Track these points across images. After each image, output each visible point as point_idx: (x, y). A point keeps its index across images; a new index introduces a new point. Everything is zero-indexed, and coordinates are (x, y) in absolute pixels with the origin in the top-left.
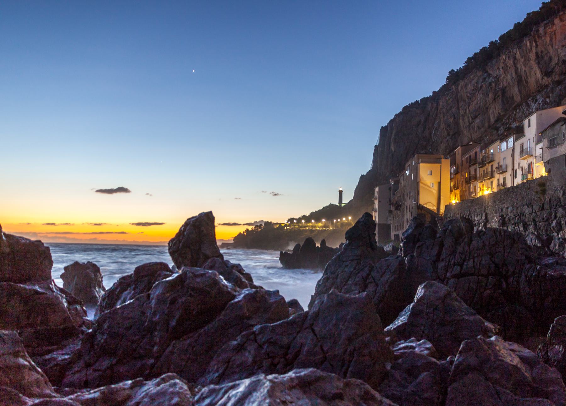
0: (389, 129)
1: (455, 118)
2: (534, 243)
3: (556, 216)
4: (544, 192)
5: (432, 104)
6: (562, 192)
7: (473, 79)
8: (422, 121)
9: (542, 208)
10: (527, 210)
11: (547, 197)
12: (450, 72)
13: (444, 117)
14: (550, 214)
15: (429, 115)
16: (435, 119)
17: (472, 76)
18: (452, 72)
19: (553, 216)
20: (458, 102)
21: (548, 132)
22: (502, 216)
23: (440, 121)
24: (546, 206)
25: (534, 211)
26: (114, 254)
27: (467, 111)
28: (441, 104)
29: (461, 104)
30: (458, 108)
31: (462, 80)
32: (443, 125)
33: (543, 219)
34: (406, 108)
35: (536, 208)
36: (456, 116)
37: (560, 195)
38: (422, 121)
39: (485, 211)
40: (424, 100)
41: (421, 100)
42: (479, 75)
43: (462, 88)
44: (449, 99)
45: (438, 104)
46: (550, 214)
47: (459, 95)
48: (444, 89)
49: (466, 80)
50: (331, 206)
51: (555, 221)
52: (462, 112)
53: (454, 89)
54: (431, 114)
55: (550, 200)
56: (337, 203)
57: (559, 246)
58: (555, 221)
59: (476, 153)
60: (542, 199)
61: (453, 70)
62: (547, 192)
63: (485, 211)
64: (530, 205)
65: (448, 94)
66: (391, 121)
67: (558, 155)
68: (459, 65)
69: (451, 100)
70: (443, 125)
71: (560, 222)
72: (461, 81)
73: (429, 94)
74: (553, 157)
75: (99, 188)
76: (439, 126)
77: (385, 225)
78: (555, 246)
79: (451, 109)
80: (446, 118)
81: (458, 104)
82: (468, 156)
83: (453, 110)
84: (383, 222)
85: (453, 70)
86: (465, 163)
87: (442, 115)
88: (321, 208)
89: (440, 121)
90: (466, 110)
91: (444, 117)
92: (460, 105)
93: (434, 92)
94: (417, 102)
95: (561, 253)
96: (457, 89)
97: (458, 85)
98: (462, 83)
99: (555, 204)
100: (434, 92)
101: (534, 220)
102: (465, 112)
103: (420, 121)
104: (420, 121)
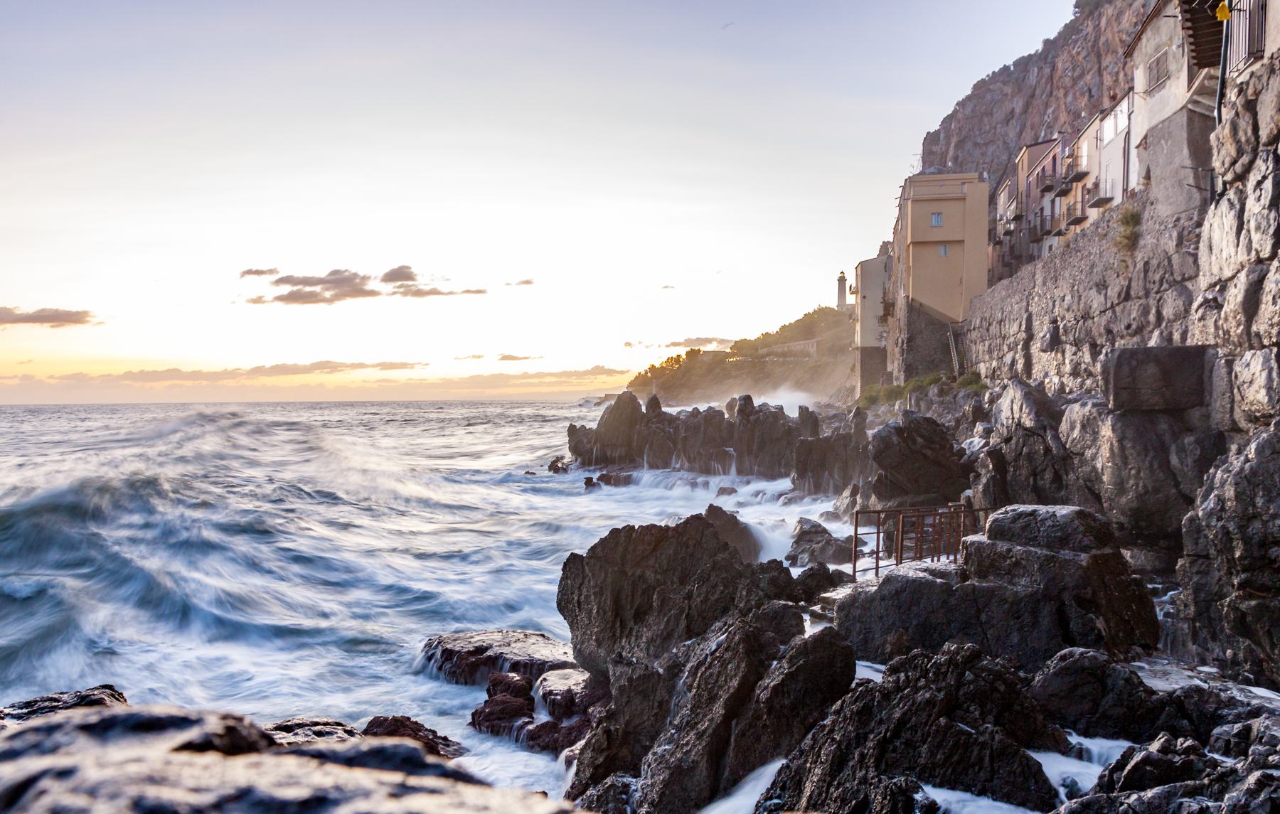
0: (942, 135)
1: (1091, 96)
2: (1017, 416)
4: (1133, 242)
5: (1040, 69)
6: (1175, 234)
8: (1018, 111)
9: (1126, 296)
10: (1096, 301)
11: (1140, 256)
13: (1066, 95)
14: (1145, 311)
16: (1047, 106)
20: (1099, 56)
21: (1144, 40)
22: (1054, 321)
24: (1136, 289)
25: (1109, 305)
26: (409, 430)
27: (1122, 75)
29: (1107, 60)
30: (1100, 75)
32: (1063, 117)
33: (1128, 327)
34: (980, 86)
35: (1113, 292)
36: (1093, 92)
37: (1171, 246)
38: (1018, 111)
39: (1027, 310)
43: (1108, 22)
44: (1078, 53)
45: (1054, 68)
46: (1145, 311)
47: (1103, 39)
50: (823, 312)
51: (1156, 333)
52: (1108, 80)
53: (1090, 29)
54: (1038, 92)
55: (1147, 264)
56: (832, 303)
57: (1083, 427)
58: (1156, 333)
59: (1054, 158)
60: (1130, 262)
62: (1142, 242)
63: (1027, 310)
64: (1102, 286)
66: (948, 120)
67: (1168, 112)
69: (1084, 54)
70: (1063, 117)
71: (1171, 334)
72: (1107, 6)
73: (1036, 46)
74: (1154, 122)
76: (1056, 119)
77: (877, 349)
78: (1073, 428)
79: (1082, 76)
80: (1070, 98)
81: (1100, 63)
82: (1039, 169)
83: (1089, 77)
84: (873, 343)
87: (1062, 92)
88: (800, 317)
89: (1058, 108)
90: (1117, 73)
91: (1066, 95)
92: (1104, 64)
94: (1006, 68)
95: (1088, 453)
96: (1097, 27)
97: (1100, 16)
99: (1157, 277)
101: (1109, 332)
102: (1117, 81)
104: (1013, 111)
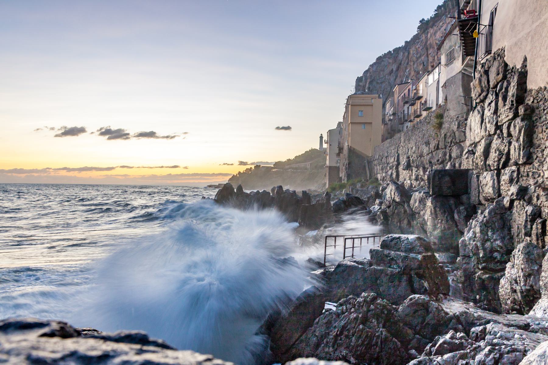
0: (364, 78)
1: (424, 65)
3: (450, 160)
4: (440, 126)
5: (404, 53)
7: (442, 27)
8: (394, 70)
9: (437, 148)
11: (443, 132)
12: (420, 21)
13: (414, 64)
14: (445, 154)
15: (400, 64)
16: (406, 68)
17: (441, 24)
18: (422, 21)
19: (447, 157)
20: (427, 49)
21: (445, 44)
23: (410, 69)
27: (436, 57)
28: (411, 52)
29: (430, 51)
30: (427, 56)
31: (432, 28)
32: (413, 73)
33: (438, 161)
36: (425, 63)
40: (397, 50)
41: (394, 50)
42: (448, 22)
43: (431, 36)
44: (419, 48)
46: (445, 154)
47: (429, 42)
48: (416, 38)
49: (435, 28)
50: (313, 151)
51: (449, 164)
52: (431, 59)
53: (424, 38)
54: (402, 62)
55: (445, 135)
56: (317, 147)
57: (420, 202)
58: (449, 164)
61: (423, 19)
62: (444, 126)
64: (428, 143)
65: (418, 42)
68: (429, 14)
69: (421, 48)
71: (455, 164)
73: (402, 44)
74: (449, 77)
75: (82, 135)
76: (410, 74)
79: (420, 57)
80: (415, 66)
81: (427, 52)
82: (403, 94)
85: (423, 19)
86: (400, 101)
89: (410, 69)
90: (434, 57)
91: (414, 64)
92: (429, 52)
93: (406, 42)
94: (390, 52)
95: (422, 213)
96: (426, 37)
98: (431, 31)
99: (450, 141)
100: (406, 42)
102: (434, 59)
103: (392, 70)
104: (392, 70)
